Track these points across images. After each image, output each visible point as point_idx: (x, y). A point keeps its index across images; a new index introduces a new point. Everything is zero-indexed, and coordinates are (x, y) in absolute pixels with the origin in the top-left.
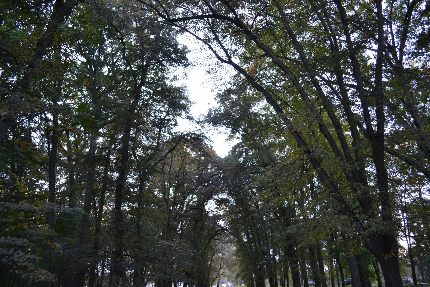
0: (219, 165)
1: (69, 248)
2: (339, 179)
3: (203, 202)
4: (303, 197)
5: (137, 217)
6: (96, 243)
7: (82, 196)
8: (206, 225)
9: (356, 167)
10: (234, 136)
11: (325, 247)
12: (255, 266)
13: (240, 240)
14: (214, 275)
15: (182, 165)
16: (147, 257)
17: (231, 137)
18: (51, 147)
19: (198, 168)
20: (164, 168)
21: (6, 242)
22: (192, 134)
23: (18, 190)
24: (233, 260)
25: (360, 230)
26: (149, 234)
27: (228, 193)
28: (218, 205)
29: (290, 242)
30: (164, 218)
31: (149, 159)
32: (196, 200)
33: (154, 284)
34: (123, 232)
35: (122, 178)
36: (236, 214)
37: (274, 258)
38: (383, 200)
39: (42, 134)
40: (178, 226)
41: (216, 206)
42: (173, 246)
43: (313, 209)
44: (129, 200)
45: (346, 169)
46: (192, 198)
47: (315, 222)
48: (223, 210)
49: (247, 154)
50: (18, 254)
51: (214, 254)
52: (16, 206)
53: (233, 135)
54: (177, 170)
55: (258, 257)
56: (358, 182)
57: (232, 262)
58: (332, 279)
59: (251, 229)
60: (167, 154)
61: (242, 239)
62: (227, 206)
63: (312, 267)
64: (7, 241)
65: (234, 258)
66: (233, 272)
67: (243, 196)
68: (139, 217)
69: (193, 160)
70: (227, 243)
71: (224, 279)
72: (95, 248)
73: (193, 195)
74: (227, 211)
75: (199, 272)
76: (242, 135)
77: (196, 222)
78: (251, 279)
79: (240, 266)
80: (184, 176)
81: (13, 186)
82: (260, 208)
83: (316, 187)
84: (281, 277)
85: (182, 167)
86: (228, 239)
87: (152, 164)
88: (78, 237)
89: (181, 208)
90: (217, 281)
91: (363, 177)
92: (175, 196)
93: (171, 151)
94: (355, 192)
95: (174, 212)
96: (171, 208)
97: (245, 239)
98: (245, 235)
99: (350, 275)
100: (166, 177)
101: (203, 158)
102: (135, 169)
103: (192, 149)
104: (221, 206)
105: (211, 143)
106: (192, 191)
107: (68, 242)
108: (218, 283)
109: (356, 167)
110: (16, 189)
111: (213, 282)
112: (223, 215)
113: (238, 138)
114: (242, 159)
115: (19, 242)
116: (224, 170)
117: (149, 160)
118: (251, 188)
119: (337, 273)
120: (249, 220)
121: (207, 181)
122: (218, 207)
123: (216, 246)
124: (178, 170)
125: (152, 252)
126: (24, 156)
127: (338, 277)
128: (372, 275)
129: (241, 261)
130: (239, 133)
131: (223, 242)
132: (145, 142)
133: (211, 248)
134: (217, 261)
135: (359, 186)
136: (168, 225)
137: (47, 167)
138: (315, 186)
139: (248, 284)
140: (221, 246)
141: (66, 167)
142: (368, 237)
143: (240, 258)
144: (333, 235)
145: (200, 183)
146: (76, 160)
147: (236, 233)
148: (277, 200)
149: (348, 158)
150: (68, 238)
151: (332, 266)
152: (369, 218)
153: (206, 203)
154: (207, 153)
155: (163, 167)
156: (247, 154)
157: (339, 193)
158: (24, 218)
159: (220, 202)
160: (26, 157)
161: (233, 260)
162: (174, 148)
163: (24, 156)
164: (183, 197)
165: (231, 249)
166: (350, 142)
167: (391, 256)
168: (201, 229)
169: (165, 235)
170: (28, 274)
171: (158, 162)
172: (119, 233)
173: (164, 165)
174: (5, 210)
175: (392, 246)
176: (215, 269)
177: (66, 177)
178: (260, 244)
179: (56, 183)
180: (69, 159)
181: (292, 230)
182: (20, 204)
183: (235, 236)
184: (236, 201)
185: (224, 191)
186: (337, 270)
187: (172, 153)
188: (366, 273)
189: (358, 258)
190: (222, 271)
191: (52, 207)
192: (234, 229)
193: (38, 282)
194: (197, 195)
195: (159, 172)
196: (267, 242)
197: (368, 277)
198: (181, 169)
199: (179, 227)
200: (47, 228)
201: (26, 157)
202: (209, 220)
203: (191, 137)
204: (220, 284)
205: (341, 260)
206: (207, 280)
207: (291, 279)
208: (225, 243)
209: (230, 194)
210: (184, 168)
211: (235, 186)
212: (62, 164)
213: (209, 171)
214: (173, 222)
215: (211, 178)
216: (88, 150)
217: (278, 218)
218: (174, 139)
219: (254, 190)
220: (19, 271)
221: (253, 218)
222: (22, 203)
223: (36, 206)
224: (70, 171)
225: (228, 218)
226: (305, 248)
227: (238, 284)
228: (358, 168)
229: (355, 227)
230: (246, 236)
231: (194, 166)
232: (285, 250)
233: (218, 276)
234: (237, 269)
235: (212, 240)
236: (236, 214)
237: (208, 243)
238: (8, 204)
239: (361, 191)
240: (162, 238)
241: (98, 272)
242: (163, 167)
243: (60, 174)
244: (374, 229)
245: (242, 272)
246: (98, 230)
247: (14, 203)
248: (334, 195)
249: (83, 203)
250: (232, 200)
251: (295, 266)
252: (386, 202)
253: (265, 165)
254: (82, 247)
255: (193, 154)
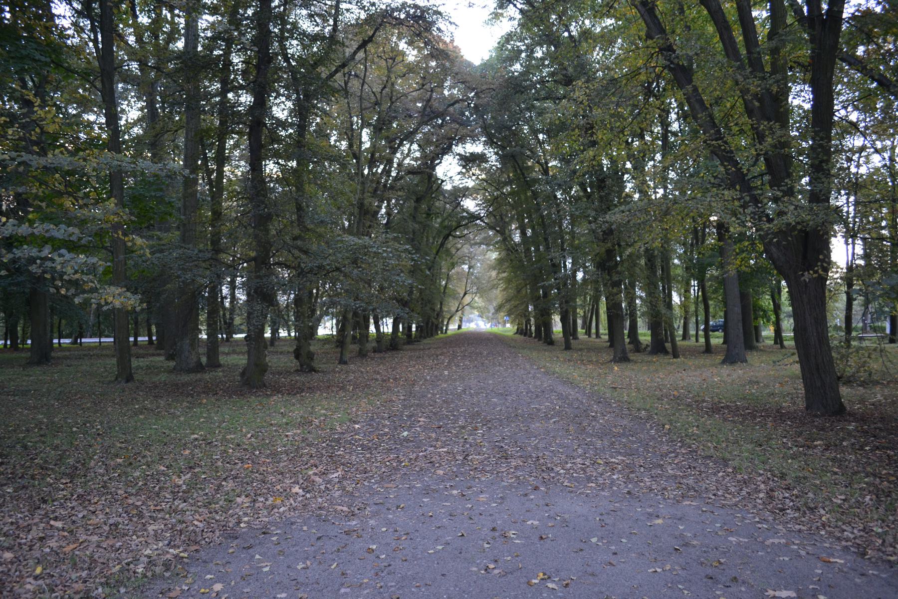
0: (469, 79)
1: (162, 251)
2: (727, 115)
3: (433, 160)
4: (646, 153)
5: (296, 187)
6: (215, 242)
7: (177, 147)
8: (439, 208)
9: (771, 85)
10: (502, 15)
11: (679, 258)
12: (535, 289)
13: (506, 238)
14: (453, 305)
15: (389, 77)
16: (320, 267)
17: (496, 16)
18: (100, 39)
19: (423, 85)
20: (350, 85)
21: (33, 234)
22: (409, 6)
23: (41, 128)
24: (490, 277)
25: (760, 220)
26: (322, 222)
27: (485, 141)
28: (464, 167)
29: (609, 245)
30: (351, 192)
31: (315, 63)
32: (418, 154)
33: (334, 321)
34: (269, 218)
35: (261, 105)
36: (499, 185)
37: (574, 276)
38: (817, 162)
39: (77, 11)
40: (380, 207)
41: (460, 169)
42: (372, 247)
43: (663, 181)
44: (276, 155)
45: (748, 90)
46: (409, 150)
47: (665, 209)
48: (474, 178)
49: (530, 57)
50: (61, 256)
51: (453, 265)
52: (42, 161)
53: (500, 11)
54: (377, 89)
55: (541, 272)
56: (769, 120)
57: (488, 282)
58: (685, 318)
59: (530, 217)
60: (355, 53)
61: (510, 236)
62: (481, 170)
63: (649, 294)
64: (35, 231)
65: (494, 273)
66: (490, 301)
67: (518, 149)
68: (300, 188)
69: (411, 69)
70: (480, 244)
71: (471, 313)
72: (213, 250)
73: (411, 145)
74: (483, 179)
75: (422, 299)
76: (521, 11)
77: (418, 200)
78: (525, 315)
79: (504, 290)
80: (392, 103)
81: (29, 117)
82: (551, 173)
83: (675, 134)
84: (585, 312)
85: (388, 84)
86: (483, 235)
87: (324, 76)
88: (178, 228)
89: (387, 172)
90: (457, 318)
91: (782, 110)
92: (373, 145)
93: (363, 45)
94: (760, 144)
95: (372, 181)
96: (366, 172)
97: (517, 238)
98: (516, 229)
99: (722, 314)
100: (355, 105)
101: (433, 64)
102: (286, 87)
103: (410, 43)
104: (470, 169)
105: (452, 28)
106: (409, 137)
107: (159, 239)
108: (461, 321)
109: (771, 85)
110: (38, 125)
111: (449, 319)
112: (473, 188)
113: (512, 19)
114: (517, 67)
115: (60, 232)
116: (479, 90)
117: (315, 65)
118: (535, 132)
119: (696, 308)
120: (526, 197)
121: (442, 115)
122: (464, 171)
123: (458, 250)
124: (379, 90)
125: (331, 258)
126: (43, 59)
127: (697, 316)
128: (766, 316)
129: (508, 281)
130: (515, 5)
131: (472, 242)
132: (306, 26)
133: (448, 253)
134: (459, 279)
135: (771, 128)
136: (361, 205)
137: (98, 84)
138: (671, 132)
139: (519, 324)
140: (467, 251)
141: (138, 85)
142: (776, 234)
143: (505, 275)
144: (698, 236)
145: (426, 119)
146: (157, 68)
147: (499, 224)
148: (591, 153)
149: (755, 64)
150: (158, 233)
151: (687, 293)
152: (783, 196)
153: (437, 162)
154: (443, 51)
155: (346, 83)
156: (530, 57)
157: (726, 143)
158: (62, 187)
159: (468, 161)
160: (48, 60)
161: (490, 277)
162: (370, 39)
163: (43, 59)
164: (391, 148)
165: (487, 257)
166: (762, 32)
167: (815, 275)
168: (428, 215)
169: (356, 226)
170: (86, 295)
171: (336, 71)
172: (263, 221)
173: (349, 78)
174: (21, 169)
175: (821, 257)
176: (454, 296)
177: (139, 106)
178: (547, 248)
179: (120, 119)
180: (143, 65)
181: (615, 217)
182: (50, 155)
183: (498, 231)
184: (502, 158)
185: (476, 136)
186: (696, 303)
187: (365, 51)
188: (755, 311)
189: (744, 278)
190: (468, 299)
191: (119, 163)
192: (495, 216)
193: (109, 309)
194: (419, 146)
195: (338, 91)
196: (563, 243)
197: (756, 318)
198: (385, 87)
199: (383, 211)
200: (113, 205)
201: (48, 60)
202: (445, 197)
203: (408, 13)
204: (464, 324)
205: (708, 284)
206: (438, 315)
207: (603, 317)
208: (476, 244)
209: (490, 142)
210: (393, 84)
211: (501, 127)
212: (128, 78)
213: (446, 93)
214: (370, 200)
215: (451, 109)
216: (180, 44)
217: (588, 196)
218: (370, 19)
219: (541, 136)
220: (67, 290)
221: (535, 195)
222: (54, 155)
223: (85, 160)
224: (145, 89)
225: (484, 195)
226: (639, 257)
227: (499, 323)
228: (775, 89)
229: (752, 213)
230: (518, 231)
231: (414, 82)
232: (598, 259)
233: (460, 308)
234: (498, 295)
235: (451, 238)
236: (499, 185)
237: (442, 245)
238: (26, 157)
239: (773, 139)
240: (349, 231)
241: (223, 298)
242: (346, 83)
243: (126, 99)
244: (790, 218)
245: (508, 301)
246: (217, 215)
247: (38, 154)
248: (715, 147)
249: (181, 163)
250: (494, 158)
251: (615, 290)
252: (824, 164)
253: (568, 81)
254: (189, 249)
255: (412, 55)
